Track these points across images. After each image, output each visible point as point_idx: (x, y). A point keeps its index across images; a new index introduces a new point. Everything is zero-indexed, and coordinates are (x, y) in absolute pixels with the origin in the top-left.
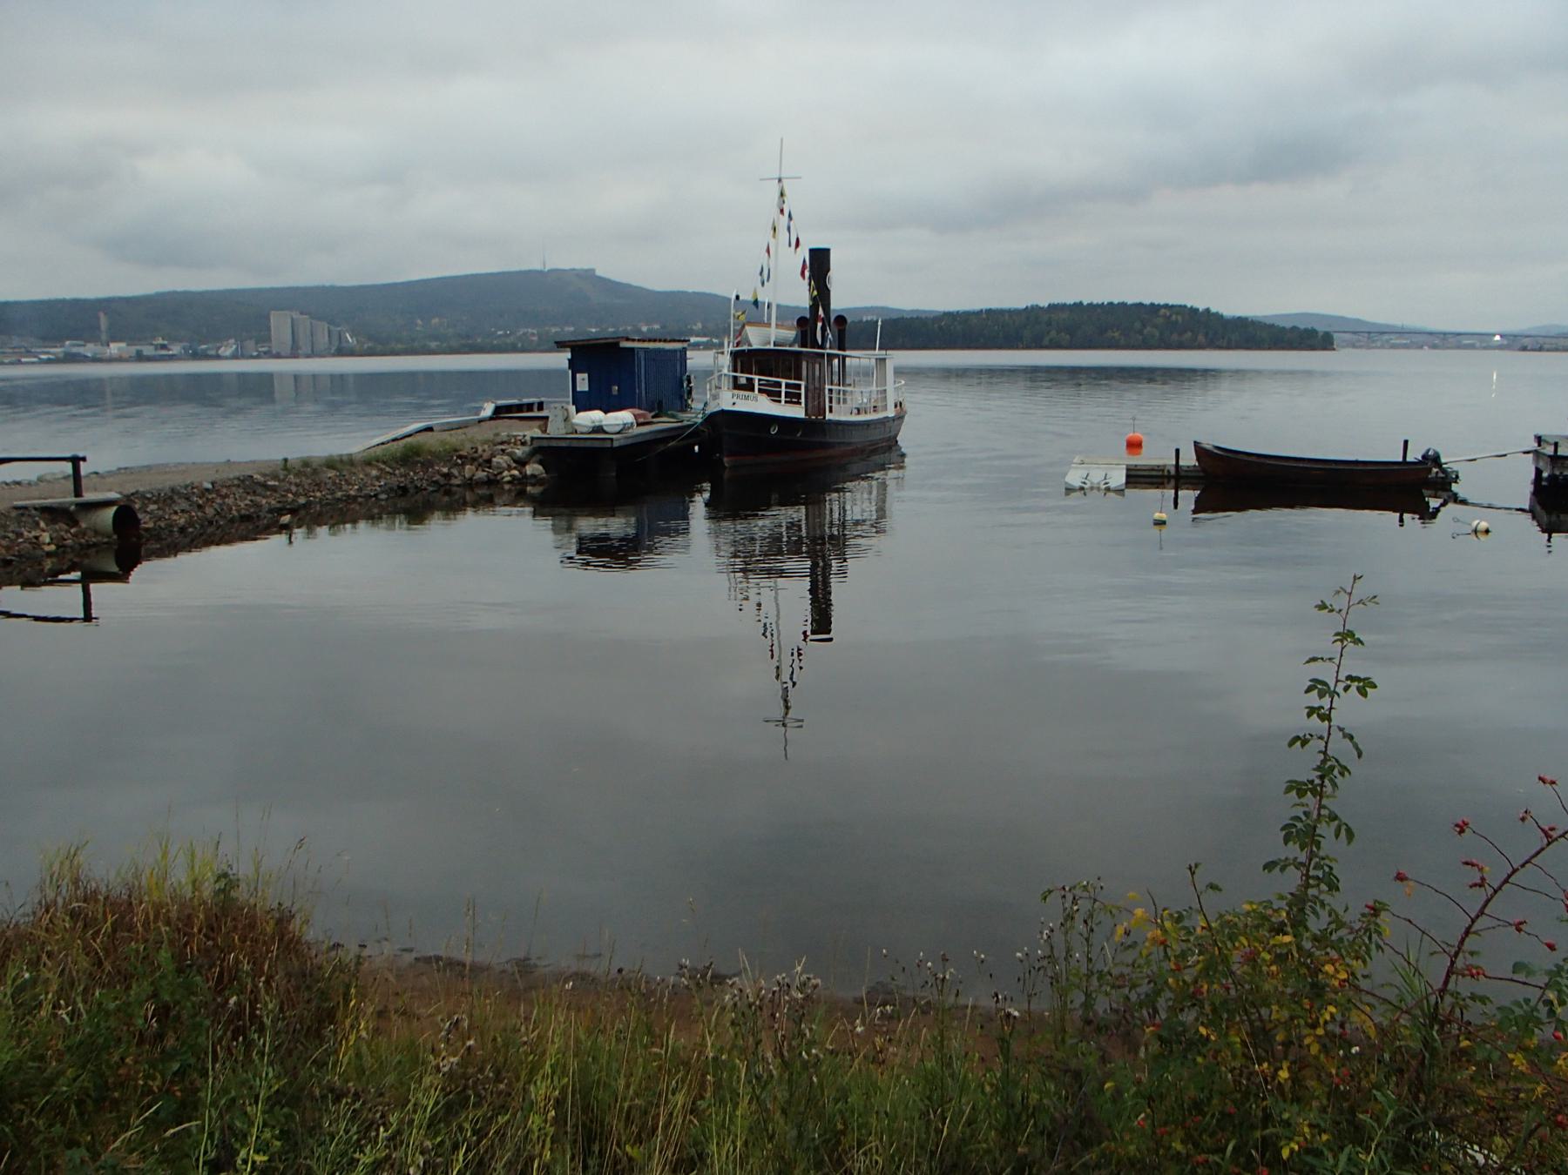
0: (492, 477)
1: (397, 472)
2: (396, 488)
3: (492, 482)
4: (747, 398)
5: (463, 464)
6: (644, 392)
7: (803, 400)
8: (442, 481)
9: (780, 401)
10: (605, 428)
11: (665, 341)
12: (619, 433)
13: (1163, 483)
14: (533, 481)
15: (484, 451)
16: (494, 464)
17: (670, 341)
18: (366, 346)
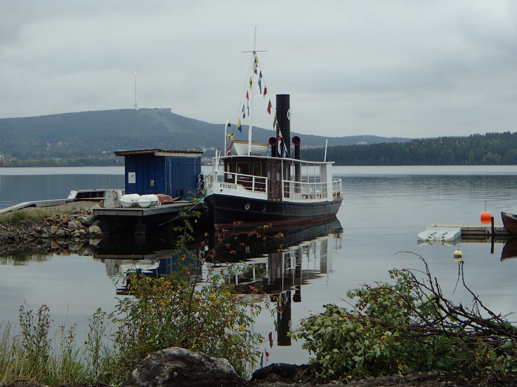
0: (68, 233)
1: (9, 229)
2: (7, 238)
3: (67, 237)
4: (230, 187)
5: (50, 225)
6: (171, 185)
7: (266, 189)
8: (37, 235)
9: (251, 189)
10: (140, 205)
11: (186, 152)
12: (148, 207)
13: (485, 239)
14: (93, 236)
15: (64, 217)
16: (69, 225)
17: (189, 153)
18: (11, 160)
